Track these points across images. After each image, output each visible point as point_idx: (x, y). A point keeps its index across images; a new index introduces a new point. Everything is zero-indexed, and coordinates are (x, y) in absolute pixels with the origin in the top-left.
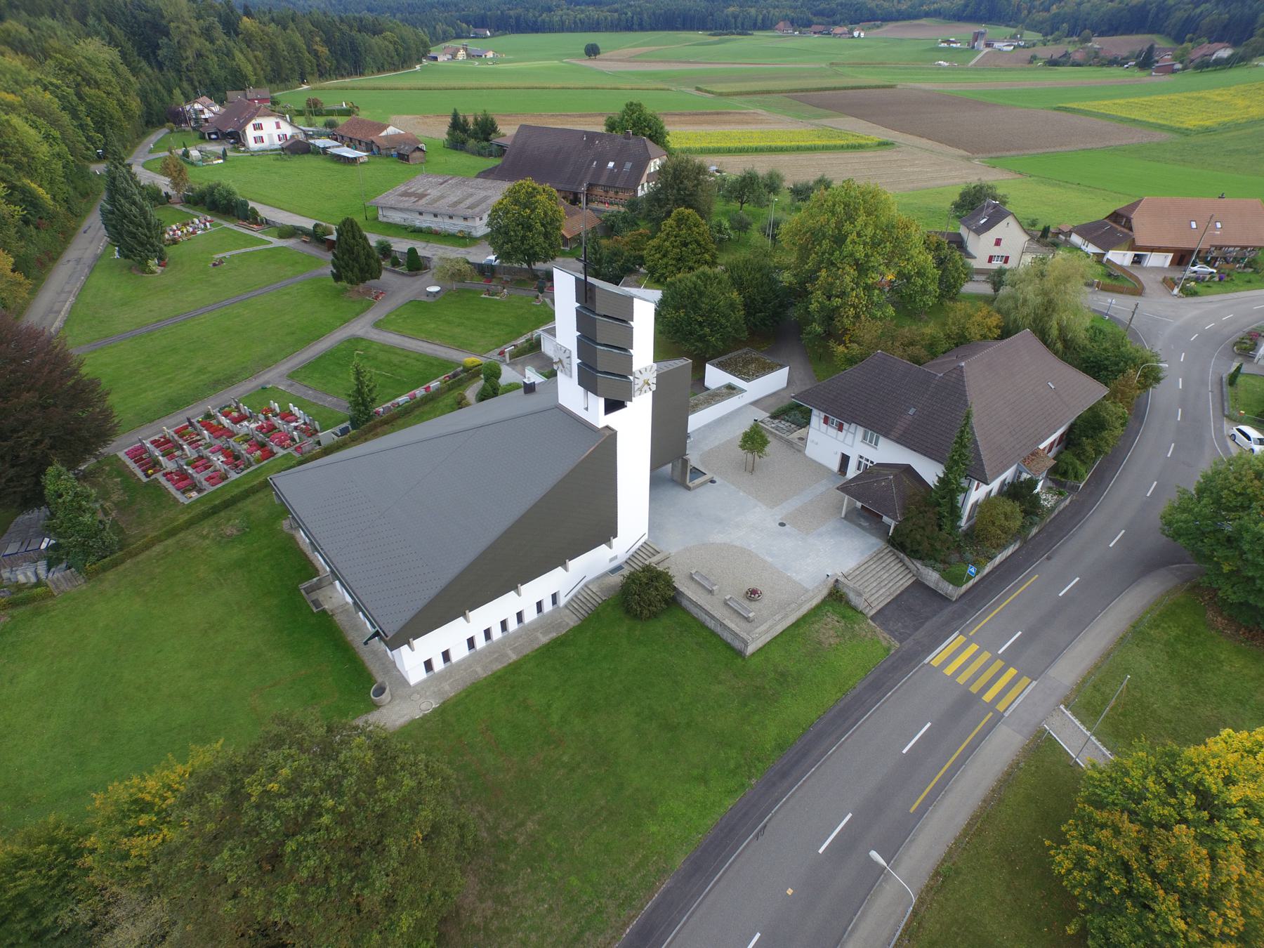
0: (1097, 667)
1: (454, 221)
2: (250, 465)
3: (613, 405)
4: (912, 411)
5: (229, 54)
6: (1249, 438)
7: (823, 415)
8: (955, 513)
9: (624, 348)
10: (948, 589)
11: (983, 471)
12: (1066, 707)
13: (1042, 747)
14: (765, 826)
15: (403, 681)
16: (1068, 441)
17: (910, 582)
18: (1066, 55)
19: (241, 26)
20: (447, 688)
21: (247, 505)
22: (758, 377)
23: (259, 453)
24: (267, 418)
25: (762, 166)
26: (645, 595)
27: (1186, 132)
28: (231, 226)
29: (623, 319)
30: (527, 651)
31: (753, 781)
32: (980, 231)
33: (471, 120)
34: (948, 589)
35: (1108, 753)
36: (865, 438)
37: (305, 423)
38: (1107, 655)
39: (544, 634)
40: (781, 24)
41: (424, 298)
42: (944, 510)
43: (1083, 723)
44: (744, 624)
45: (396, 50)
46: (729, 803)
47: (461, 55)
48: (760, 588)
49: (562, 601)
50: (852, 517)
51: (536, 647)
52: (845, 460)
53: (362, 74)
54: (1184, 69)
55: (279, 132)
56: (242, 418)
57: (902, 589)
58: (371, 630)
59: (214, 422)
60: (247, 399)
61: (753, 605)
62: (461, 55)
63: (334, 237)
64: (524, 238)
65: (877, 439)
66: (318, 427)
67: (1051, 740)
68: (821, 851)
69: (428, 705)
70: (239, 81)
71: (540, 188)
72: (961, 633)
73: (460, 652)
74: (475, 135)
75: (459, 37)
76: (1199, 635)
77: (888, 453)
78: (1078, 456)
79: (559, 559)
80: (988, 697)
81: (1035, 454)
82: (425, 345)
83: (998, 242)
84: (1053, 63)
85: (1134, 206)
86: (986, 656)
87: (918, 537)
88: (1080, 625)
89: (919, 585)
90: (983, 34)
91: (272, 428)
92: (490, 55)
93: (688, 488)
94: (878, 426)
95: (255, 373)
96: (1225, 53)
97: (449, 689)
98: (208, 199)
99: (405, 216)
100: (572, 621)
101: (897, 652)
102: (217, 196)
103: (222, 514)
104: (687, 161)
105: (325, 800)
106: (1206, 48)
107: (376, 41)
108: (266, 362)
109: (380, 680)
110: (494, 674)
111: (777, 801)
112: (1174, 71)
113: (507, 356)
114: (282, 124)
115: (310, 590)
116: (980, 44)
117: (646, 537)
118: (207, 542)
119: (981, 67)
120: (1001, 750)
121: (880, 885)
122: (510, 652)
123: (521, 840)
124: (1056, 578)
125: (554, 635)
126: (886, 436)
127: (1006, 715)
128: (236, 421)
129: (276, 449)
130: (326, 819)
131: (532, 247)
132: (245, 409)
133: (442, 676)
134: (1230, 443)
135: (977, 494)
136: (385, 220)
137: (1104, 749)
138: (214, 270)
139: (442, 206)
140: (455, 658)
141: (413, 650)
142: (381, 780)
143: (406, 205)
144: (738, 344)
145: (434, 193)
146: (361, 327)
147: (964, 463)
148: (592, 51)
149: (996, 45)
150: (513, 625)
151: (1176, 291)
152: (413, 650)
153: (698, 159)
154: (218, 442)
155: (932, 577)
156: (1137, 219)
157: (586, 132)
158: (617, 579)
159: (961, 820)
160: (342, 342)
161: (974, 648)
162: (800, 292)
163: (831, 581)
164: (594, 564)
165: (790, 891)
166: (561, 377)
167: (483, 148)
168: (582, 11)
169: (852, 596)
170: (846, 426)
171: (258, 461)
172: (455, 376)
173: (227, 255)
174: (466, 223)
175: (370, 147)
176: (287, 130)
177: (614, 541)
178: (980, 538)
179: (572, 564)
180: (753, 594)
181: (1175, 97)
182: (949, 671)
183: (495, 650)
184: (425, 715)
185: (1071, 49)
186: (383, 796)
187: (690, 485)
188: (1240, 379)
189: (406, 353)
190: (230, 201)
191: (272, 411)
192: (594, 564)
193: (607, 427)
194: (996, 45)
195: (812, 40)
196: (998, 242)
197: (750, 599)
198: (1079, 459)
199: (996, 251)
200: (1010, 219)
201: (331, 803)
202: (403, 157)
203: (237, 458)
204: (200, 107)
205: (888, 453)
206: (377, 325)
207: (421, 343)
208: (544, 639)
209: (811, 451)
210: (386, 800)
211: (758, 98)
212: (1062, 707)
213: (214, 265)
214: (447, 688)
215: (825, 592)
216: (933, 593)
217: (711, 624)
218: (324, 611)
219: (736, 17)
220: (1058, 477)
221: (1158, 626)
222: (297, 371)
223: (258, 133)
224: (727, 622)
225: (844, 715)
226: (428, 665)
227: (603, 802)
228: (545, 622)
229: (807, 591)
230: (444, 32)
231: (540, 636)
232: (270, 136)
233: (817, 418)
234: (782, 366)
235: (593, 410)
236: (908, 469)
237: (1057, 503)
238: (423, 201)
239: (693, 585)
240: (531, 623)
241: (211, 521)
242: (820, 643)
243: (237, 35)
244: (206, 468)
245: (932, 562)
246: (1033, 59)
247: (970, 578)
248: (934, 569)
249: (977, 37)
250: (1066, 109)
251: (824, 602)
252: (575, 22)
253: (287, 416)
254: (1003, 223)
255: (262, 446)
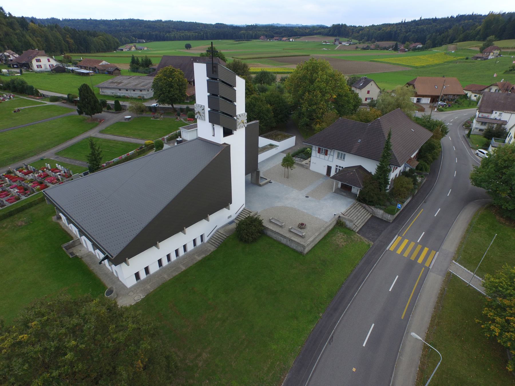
0: (461, 243)
1: (136, 92)
2: (34, 192)
3: (227, 132)
4: (359, 141)
5: (23, 36)
6: (484, 153)
7: (317, 147)
8: (386, 182)
9: (231, 100)
10: (389, 217)
11: (397, 161)
12: (456, 261)
13: (451, 280)
14: (332, 337)
15: (124, 286)
16: (419, 157)
17: (370, 216)
18: (368, 46)
19: (30, 26)
20: (149, 287)
21: (32, 210)
22: (283, 140)
23: (39, 187)
24: (43, 171)
25: (270, 69)
26: (249, 230)
27: (417, 67)
28: (25, 98)
29: (231, 86)
30: (191, 264)
31: (321, 315)
32: (361, 88)
33: (140, 60)
34: (389, 217)
35: (481, 279)
36: (338, 157)
37: (65, 172)
38: (464, 237)
39: (199, 256)
40: (262, 37)
41: (124, 121)
42: (382, 181)
43: (465, 267)
44: (303, 240)
45: (105, 43)
46: (311, 327)
47: (133, 49)
48: (305, 223)
49: (206, 239)
50: (338, 191)
51: (195, 262)
52: (329, 168)
53: (90, 53)
54: (409, 50)
55: (49, 63)
56: (29, 172)
57: (367, 219)
58: (102, 256)
59: (13, 175)
60: (32, 164)
61: (302, 231)
62: (133, 49)
63: (78, 99)
64: (169, 91)
65: (345, 155)
66: (71, 173)
67: (454, 276)
68: (364, 345)
69: (139, 297)
70: (28, 46)
71: (176, 70)
72: (399, 235)
73: (154, 268)
74: (142, 65)
75: (132, 42)
76: (496, 226)
77: (351, 161)
78: (425, 161)
79: (203, 215)
80: (420, 261)
81: (411, 159)
82: (125, 138)
83: (368, 92)
84: (364, 49)
85: (415, 80)
86: (413, 244)
87: (372, 194)
88: (448, 227)
89: (374, 217)
90: (338, 39)
91: (47, 176)
92: (146, 49)
93: (260, 186)
94: (344, 147)
95: (36, 154)
96: (421, 46)
97: (150, 288)
98: (11, 86)
99: (113, 91)
100: (212, 248)
101: (373, 246)
102: (16, 84)
103: (16, 216)
104: (239, 62)
105: (69, 342)
106: (414, 45)
107: (95, 39)
108: (44, 148)
109: (109, 287)
110: (174, 277)
111: (335, 323)
112: (406, 51)
113: (166, 140)
114: (51, 60)
115: (68, 248)
116: (337, 43)
117: (244, 206)
118: (6, 230)
119: (339, 50)
120: (433, 285)
121: (399, 358)
122: (181, 266)
123: (200, 364)
124: (430, 210)
125: (204, 256)
126: (349, 152)
127: (431, 268)
128: (26, 174)
129: (48, 184)
130: (69, 356)
131: (173, 95)
132: (31, 168)
133: (145, 281)
134: (477, 157)
135: (393, 175)
136: (103, 94)
137: (478, 277)
138: (15, 114)
139: (129, 86)
140: (152, 271)
141: (128, 265)
142: (112, 327)
143: (113, 86)
144: (272, 129)
145: (125, 82)
146: (94, 133)
147: (386, 161)
148: (188, 47)
149: (343, 43)
150: (182, 253)
151: (436, 110)
152: (128, 265)
153: (243, 62)
154: (15, 184)
155: (380, 213)
156: (415, 84)
157: (192, 57)
158: (234, 226)
159: (427, 320)
160: (84, 139)
161: (406, 241)
162: (295, 106)
163: (337, 217)
164: (221, 219)
165: (354, 370)
166: (199, 122)
167: (146, 70)
168: (183, 33)
169: (348, 223)
170: (329, 151)
171: (38, 190)
172: (141, 148)
173: (22, 108)
174: (141, 93)
175: (94, 69)
176: (54, 63)
177: (231, 206)
178: (398, 192)
179: (212, 217)
180: (302, 226)
181: (409, 57)
182: (399, 251)
183: (173, 266)
184: (137, 303)
185: (369, 45)
186: (115, 336)
187: (261, 184)
188: (471, 136)
189: (117, 142)
190: (23, 86)
191: (47, 168)
192: (221, 219)
193: (225, 144)
194: (343, 43)
195: (273, 42)
196: (368, 92)
197: (301, 228)
198: (426, 162)
199: (368, 96)
200: (372, 83)
201: (73, 343)
202: (110, 73)
203: (26, 189)
204: (8, 54)
205: (351, 161)
206: (101, 132)
207: (123, 138)
208: (199, 258)
209: (313, 167)
210: (116, 339)
211: (256, 60)
212: (454, 261)
213: (15, 112)
214: (149, 287)
215: (335, 223)
216: (381, 221)
217: (284, 241)
218: (76, 257)
219: (244, 34)
220: (418, 171)
221: (480, 224)
222: (60, 151)
223: (39, 63)
224: (293, 238)
225: (357, 277)
226: (137, 275)
227: (244, 337)
228: (197, 251)
229: (326, 222)
230: (125, 41)
231: (197, 257)
232: (45, 65)
233: (314, 152)
234: (292, 136)
235: (218, 136)
236: (360, 167)
237: (422, 180)
238: (121, 85)
239: (272, 225)
240: (191, 251)
241: (8, 220)
242: (338, 245)
243: (28, 30)
244: (7, 196)
245: (379, 206)
246: (357, 48)
247: (398, 210)
248: (381, 209)
249: (335, 40)
250: (374, 61)
251: (334, 227)
252: (180, 37)
253: (55, 170)
254: (370, 84)
255: (41, 183)
